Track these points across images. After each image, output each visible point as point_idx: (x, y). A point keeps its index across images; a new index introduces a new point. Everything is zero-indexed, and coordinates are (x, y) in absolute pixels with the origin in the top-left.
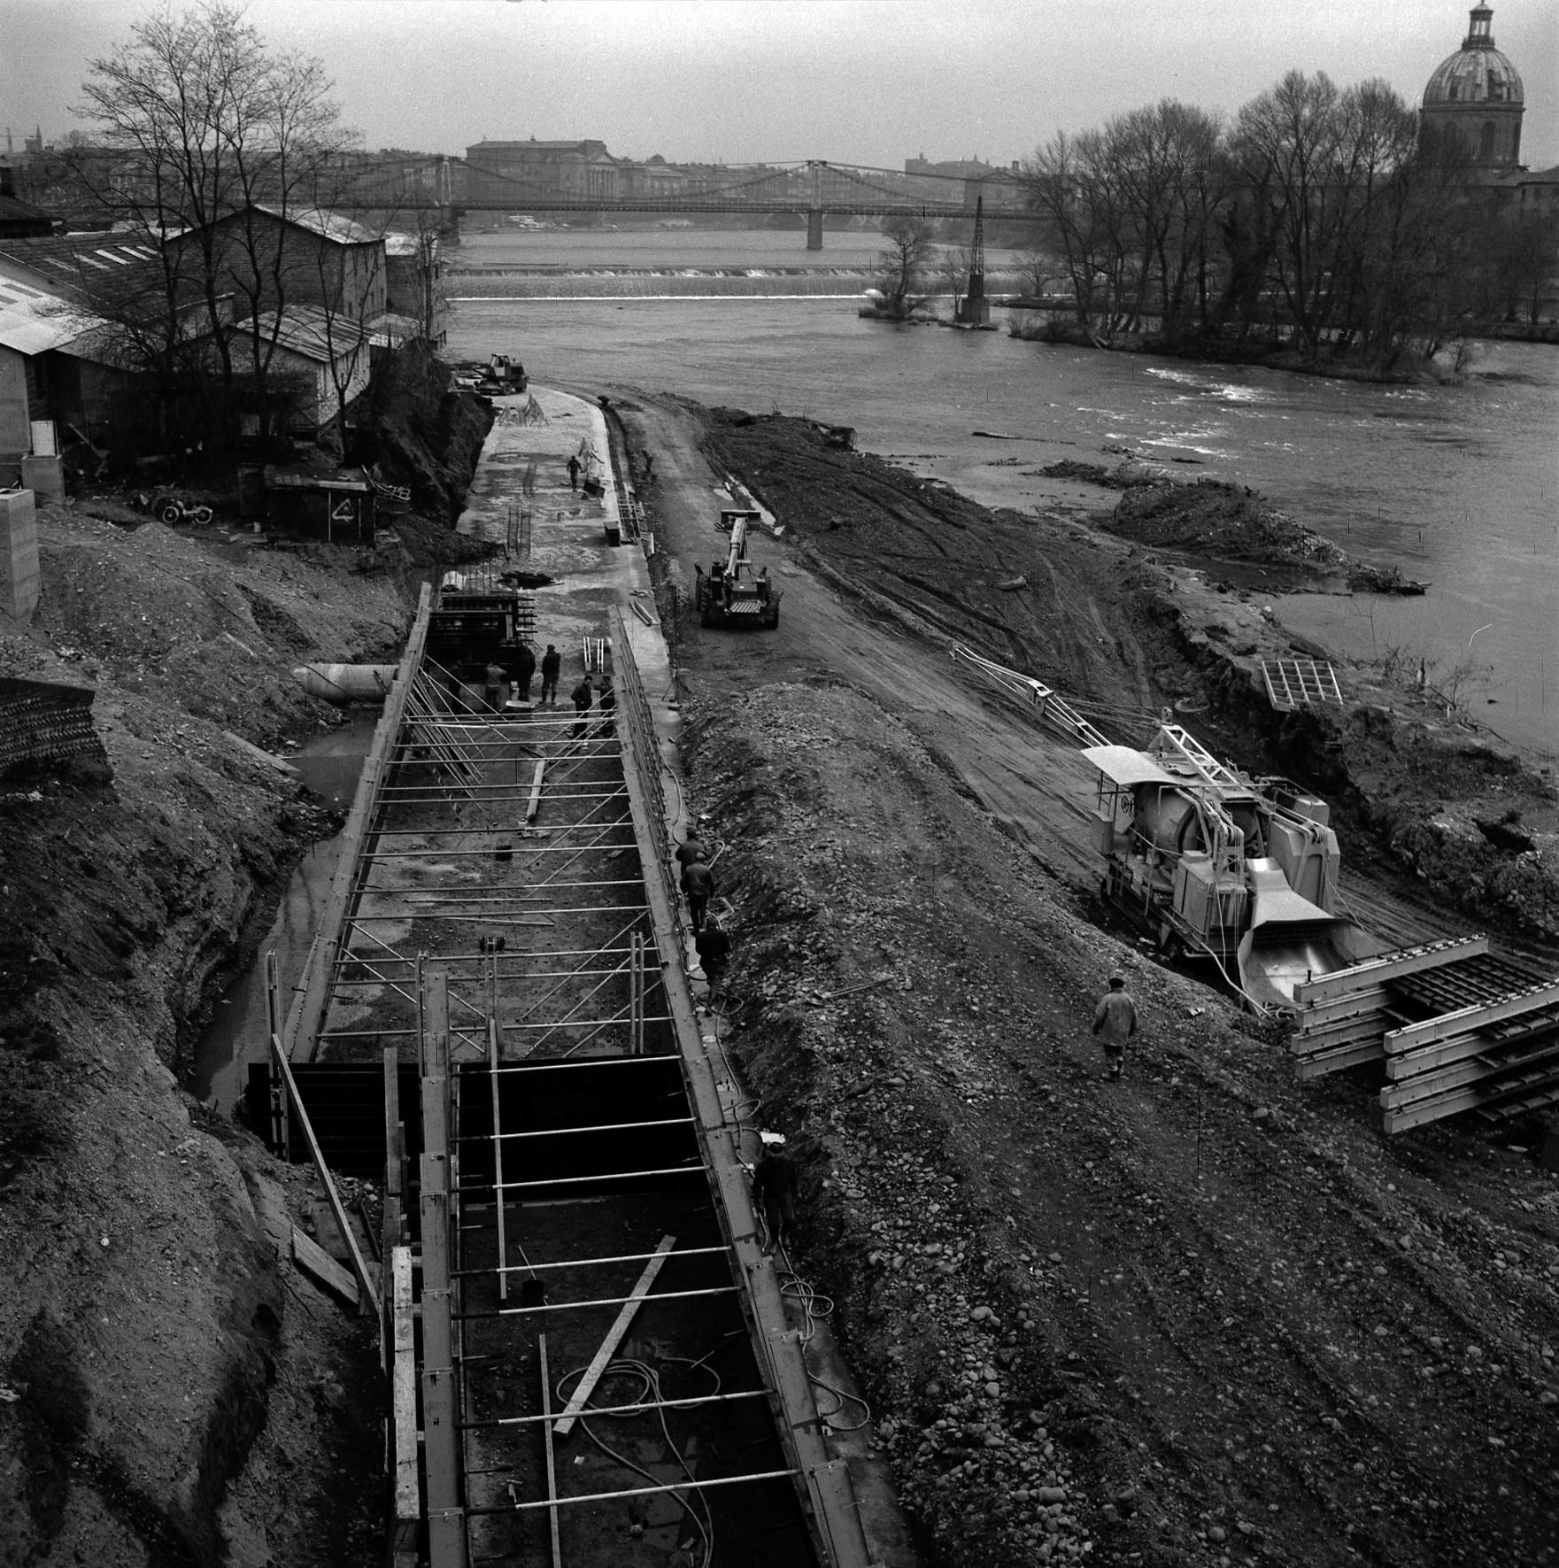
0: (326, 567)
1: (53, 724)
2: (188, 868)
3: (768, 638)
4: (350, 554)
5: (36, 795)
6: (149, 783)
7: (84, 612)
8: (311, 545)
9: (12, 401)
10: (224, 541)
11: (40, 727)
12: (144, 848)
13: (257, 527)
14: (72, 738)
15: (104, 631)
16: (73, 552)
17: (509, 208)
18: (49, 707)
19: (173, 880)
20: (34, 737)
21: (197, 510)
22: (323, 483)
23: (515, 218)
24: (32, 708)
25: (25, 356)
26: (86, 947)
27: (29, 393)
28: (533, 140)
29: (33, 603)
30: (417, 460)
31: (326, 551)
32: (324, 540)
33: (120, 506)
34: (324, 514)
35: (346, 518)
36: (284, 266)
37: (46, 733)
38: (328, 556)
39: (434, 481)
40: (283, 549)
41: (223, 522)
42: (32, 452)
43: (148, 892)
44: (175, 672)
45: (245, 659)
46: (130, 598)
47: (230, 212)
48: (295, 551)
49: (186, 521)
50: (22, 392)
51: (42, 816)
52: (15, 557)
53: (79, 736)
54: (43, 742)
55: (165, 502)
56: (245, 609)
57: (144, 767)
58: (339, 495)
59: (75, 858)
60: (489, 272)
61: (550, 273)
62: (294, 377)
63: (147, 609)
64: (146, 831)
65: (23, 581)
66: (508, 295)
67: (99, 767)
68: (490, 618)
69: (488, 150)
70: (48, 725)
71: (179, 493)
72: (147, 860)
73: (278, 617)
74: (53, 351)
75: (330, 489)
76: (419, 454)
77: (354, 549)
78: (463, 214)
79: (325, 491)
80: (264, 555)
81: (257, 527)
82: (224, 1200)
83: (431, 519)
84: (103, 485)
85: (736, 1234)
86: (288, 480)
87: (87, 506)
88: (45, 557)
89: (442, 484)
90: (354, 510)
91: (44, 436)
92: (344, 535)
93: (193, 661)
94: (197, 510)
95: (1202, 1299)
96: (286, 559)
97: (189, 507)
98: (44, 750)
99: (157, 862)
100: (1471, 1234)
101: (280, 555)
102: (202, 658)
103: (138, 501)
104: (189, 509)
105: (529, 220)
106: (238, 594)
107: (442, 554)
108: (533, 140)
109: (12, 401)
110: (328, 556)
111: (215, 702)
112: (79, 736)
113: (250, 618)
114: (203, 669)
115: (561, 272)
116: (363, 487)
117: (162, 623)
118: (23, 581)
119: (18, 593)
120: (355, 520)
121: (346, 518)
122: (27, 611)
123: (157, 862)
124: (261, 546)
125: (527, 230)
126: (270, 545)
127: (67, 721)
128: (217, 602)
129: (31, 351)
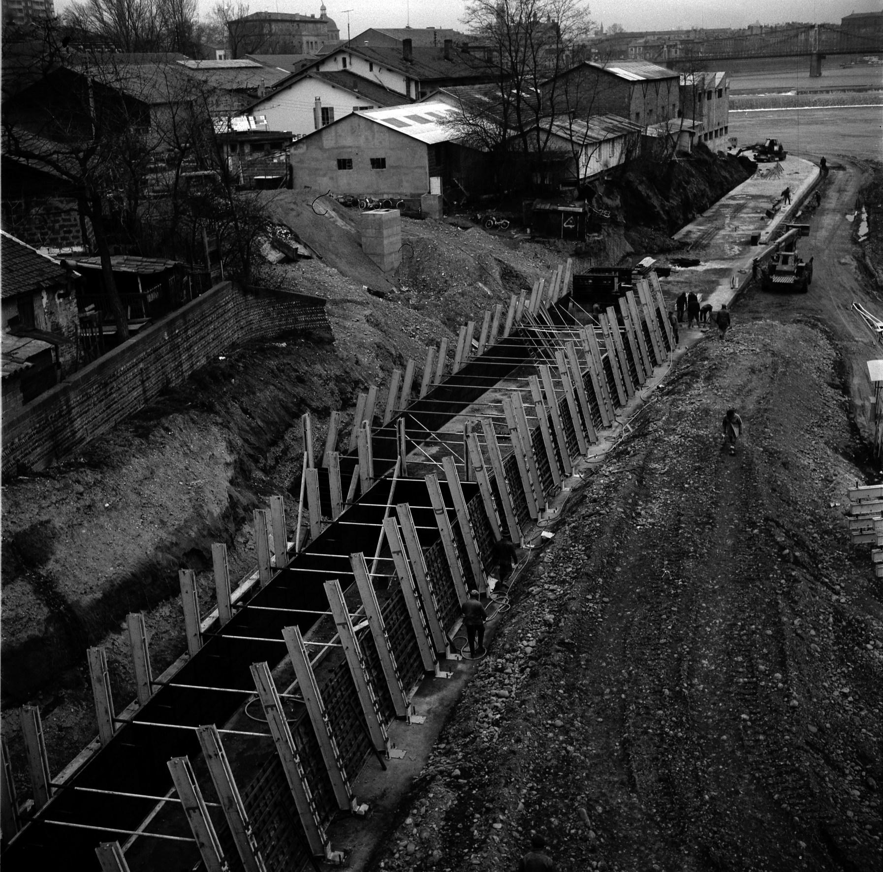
0: (559, 252)
1: (306, 314)
2: (360, 385)
3: (797, 300)
4: (572, 245)
5: (284, 345)
6: (361, 345)
7: (417, 270)
8: (552, 240)
9: (421, 167)
10: (511, 238)
11: (300, 315)
12: (338, 373)
13: (528, 231)
14: (315, 321)
15: (424, 280)
16: (420, 240)
17: (864, 52)
18: (304, 306)
19: (350, 389)
20: (296, 320)
21: (502, 222)
22: (561, 208)
23: (867, 58)
24: (295, 306)
25: (427, 144)
26: (267, 410)
27: (430, 163)
28: (408, 27)
29: (396, 265)
30: (648, 197)
31: (559, 244)
32: (559, 238)
33: (467, 220)
34: (560, 224)
35: (571, 226)
36: (555, 95)
37: (302, 318)
38: (560, 246)
39: (658, 209)
40: (538, 242)
41: (515, 228)
42: (429, 193)
43: (332, 393)
44: (446, 300)
45: (485, 295)
46: (439, 264)
47: (324, 69)
48: (543, 243)
49: (495, 227)
50: (426, 162)
51: (282, 354)
52: (386, 242)
53: (318, 320)
54: (301, 322)
55: (488, 218)
56: (496, 272)
57: (362, 338)
58: (568, 214)
59: (294, 374)
60: (822, 92)
61: (860, 91)
62: (562, 153)
63: (446, 269)
64: (342, 366)
65: (391, 254)
66: (838, 104)
67: (328, 336)
68: (606, 278)
69: (855, 19)
70: (304, 314)
71: (494, 214)
72: (338, 379)
73: (517, 276)
74: (448, 142)
75: (563, 211)
76: (650, 194)
77: (574, 243)
78: (825, 58)
79: (561, 212)
80: (527, 245)
81: (528, 231)
82: (201, 506)
83: (655, 230)
84: (460, 210)
85: (392, 550)
86: (543, 207)
87: (451, 219)
88: (405, 244)
89: (664, 210)
90: (575, 222)
91: (436, 185)
92: (569, 235)
93: (458, 295)
94: (502, 222)
95: (659, 629)
96: (538, 247)
97: (498, 220)
98: (301, 326)
99: (344, 381)
100: (862, 629)
101: (536, 245)
102: (462, 294)
103: (477, 217)
104: (498, 220)
105: (875, 59)
106: (494, 264)
107: (651, 248)
108: (408, 27)
109: (421, 167)
110: (560, 246)
111: (461, 316)
112: (318, 320)
113: (497, 276)
114: (461, 300)
115: (866, 90)
116: (581, 210)
117: (451, 277)
118: (391, 254)
119: (387, 260)
120: (576, 227)
121: (571, 226)
122: (392, 269)
123: (344, 381)
124: (527, 241)
125: (872, 65)
126: (532, 240)
127: (313, 313)
128: (482, 267)
129: (430, 142)
